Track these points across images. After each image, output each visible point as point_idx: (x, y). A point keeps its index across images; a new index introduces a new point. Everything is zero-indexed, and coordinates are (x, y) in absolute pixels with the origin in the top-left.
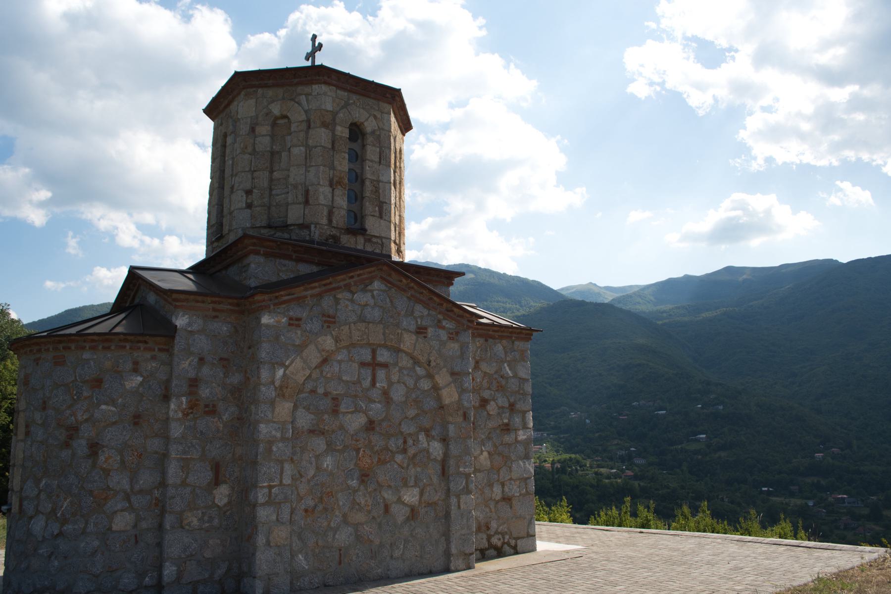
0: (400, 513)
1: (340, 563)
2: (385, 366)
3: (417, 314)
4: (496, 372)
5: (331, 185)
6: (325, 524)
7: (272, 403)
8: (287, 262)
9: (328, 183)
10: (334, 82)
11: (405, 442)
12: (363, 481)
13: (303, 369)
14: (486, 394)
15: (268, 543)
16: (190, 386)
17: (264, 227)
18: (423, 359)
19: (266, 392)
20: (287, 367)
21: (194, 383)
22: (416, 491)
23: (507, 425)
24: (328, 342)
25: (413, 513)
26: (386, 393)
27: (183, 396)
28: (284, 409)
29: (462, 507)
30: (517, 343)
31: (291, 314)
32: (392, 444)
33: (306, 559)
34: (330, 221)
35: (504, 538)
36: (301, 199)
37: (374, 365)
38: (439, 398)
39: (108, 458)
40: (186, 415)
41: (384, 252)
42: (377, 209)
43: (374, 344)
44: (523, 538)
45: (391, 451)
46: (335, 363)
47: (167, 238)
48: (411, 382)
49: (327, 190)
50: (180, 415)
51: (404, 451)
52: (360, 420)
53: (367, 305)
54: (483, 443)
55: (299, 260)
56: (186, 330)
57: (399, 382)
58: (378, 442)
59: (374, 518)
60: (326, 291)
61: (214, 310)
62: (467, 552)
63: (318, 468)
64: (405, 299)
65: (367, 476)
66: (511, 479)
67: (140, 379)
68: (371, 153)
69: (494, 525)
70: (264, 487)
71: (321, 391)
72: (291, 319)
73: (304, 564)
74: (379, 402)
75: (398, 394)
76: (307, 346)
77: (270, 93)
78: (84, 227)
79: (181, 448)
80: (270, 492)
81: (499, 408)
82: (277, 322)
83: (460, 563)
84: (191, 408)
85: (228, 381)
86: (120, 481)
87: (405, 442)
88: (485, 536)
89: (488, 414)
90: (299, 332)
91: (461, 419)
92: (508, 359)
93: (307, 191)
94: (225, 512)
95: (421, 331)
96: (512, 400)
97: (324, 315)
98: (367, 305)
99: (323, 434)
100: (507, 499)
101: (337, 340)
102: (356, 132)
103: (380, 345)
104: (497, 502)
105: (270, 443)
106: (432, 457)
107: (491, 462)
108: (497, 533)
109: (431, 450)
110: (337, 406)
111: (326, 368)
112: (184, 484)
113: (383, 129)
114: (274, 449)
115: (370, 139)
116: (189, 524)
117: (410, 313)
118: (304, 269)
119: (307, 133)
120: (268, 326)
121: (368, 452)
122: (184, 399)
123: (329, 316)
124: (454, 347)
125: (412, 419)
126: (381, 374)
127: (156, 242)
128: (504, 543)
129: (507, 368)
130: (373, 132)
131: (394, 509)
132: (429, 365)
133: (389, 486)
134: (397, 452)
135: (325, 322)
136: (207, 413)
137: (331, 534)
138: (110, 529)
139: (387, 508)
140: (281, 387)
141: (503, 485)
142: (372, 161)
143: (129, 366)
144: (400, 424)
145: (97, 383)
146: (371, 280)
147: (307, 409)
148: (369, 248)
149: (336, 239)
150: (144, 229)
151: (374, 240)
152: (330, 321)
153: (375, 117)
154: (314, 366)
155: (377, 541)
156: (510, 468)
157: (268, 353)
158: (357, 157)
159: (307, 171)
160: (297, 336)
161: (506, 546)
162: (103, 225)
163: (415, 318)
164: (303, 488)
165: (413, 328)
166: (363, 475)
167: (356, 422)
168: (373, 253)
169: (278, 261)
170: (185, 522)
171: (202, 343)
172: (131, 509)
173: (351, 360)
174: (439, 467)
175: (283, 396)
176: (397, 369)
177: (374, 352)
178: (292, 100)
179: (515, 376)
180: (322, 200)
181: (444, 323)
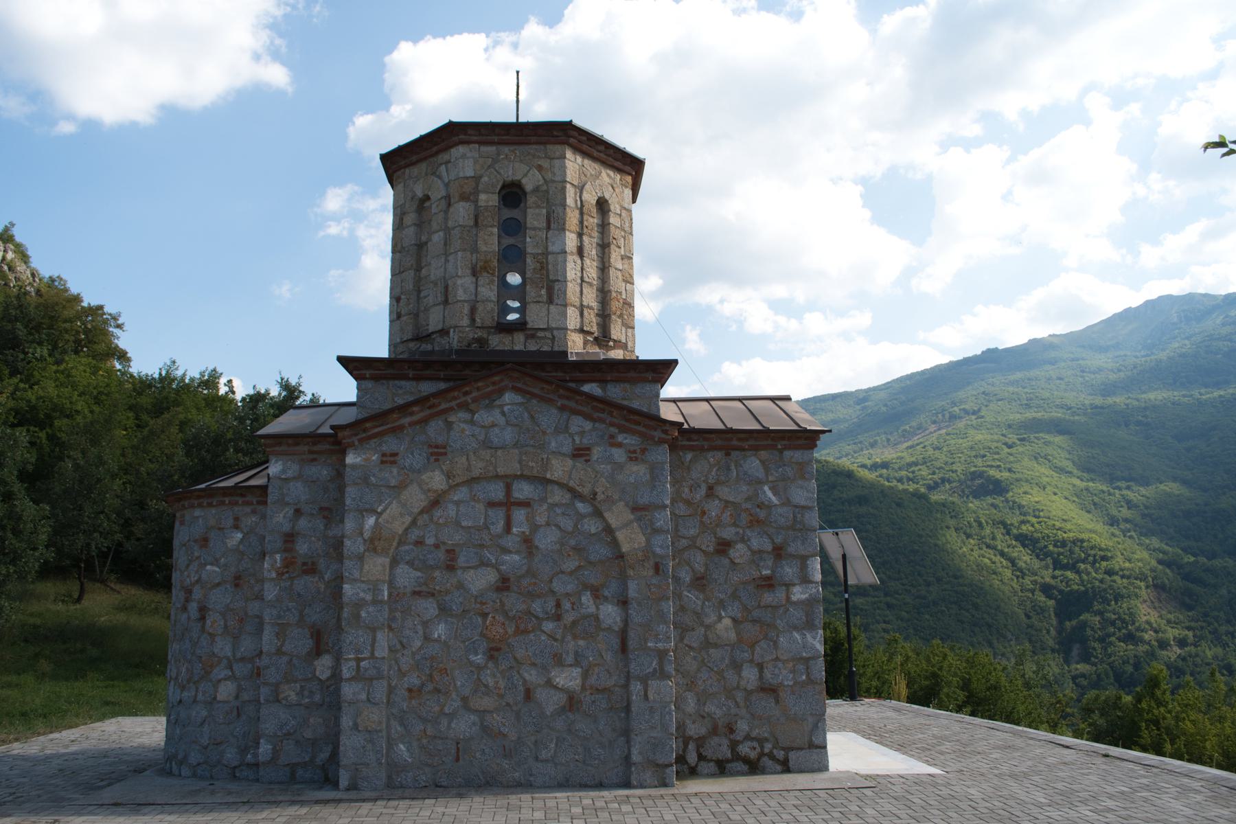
0: (550, 702)
1: (457, 760)
2: (525, 504)
3: (573, 429)
4: (748, 499)
5: (474, 273)
6: (437, 709)
7: (360, 558)
8: (403, 383)
9: (469, 272)
10: (475, 138)
11: (558, 605)
12: (491, 657)
13: (402, 515)
14: (728, 533)
15: (356, 726)
16: (286, 542)
17: (412, 340)
18: (586, 491)
19: (352, 546)
20: (380, 514)
21: (290, 538)
22: (576, 672)
23: (769, 578)
24: (437, 480)
25: (572, 702)
26: (527, 541)
27: (277, 552)
28: (376, 566)
29: (651, 697)
30: (788, 454)
31: (384, 448)
32: (537, 607)
33: (408, 750)
34: (473, 320)
35: (762, 747)
36: (440, 298)
37: (509, 504)
38: (615, 543)
39: (214, 621)
40: (280, 574)
41: (556, 349)
42: (543, 292)
43: (506, 476)
44: (802, 749)
45: (537, 618)
46: (450, 506)
47: (807, 316)
48: (567, 524)
49: (468, 281)
50: (274, 575)
51: (558, 618)
52: (487, 577)
53: (494, 425)
54: (722, 604)
55: (418, 378)
56: (280, 479)
57: (548, 524)
58: (514, 603)
59: (508, 704)
60: (432, 416)
61: (311, 452)
62: (661, 762)
63: (427, 638)
64: (555, 411)
65: (498, 650)
66: (777, 659)
67: (240, 535)
68: (534, 217)
69: (742, 727)
70: (350, 659)
71: (430, 541)
72: (384, 455)
73: (406, 755)
74: (518, 552)
75: (547, 540)
76: (406, 486)
77: (415, 171)
78: (701, 315)
79: (275, 612)
80: (358, 666)
81: (754, 552)
82: (366, 460)
83: (648, 776)
84: (287, 567)
85: (330, 533)
86: (223, 647)
87: (558, 605)
88: (725, 742)
89: (732, 562)
90: (395, 471)
91: (651, 572)
92: (770, 478)
93: (446, 287)
94: (328, 687)
95: (581, 453)
96: (779, 540)
97: (430, 446)
98: (494, 425)
99: (433, 595)
100: (771, 690)
101: (449, 476)
102: (512, 194)
103: (516, 477)
104: (749, 693)
105: (359, 604)
106: (604, 626)
107: (738, 634)
108: (748, 737)
109: (601, 617)
110: (452, 560)
111: (438, 513)
112: (279, 652)
113: (554, 181)
114: (363, 614)
115: (531, 200)
116: (286, 698)
117: (563, 429)
118: (427, 388)
119: (446, 212)
120: (354, 467)
121: (500, 618)
122: (278, 557)
123: (437, 447)
124: (638, 471)
125: (571, 573)
126: (519, 515)
127: (794, 324)
128: (762, 754)
129: (770, 494)
130: (536, 190)
131: (541, 695)
132: (594, 499)
133: (534, 665)
134: (547, 619)
135: (432, 454)
136: (306, 572)
137: (445, 722)
138: (215, 698)
139: (528, 695)
140: (372, 540)
141: (761, 667)
142: (534, 229)
143: (230, 522)
144: (551, 581)
145: (204, 541)
146: (501, 392)
147: (410, 563)
148: (532, 347)
149: (482, 342)
150: (776, 306)
151: (540, 334)
152: (438, 453)
153: (540, 168)
154: (416, 511)
155: (513, 736)
156: (775, 643)
157: (354, 499)
158: (512, 228)
159: (447, 261)
160: (392, 475)
161: (765, 759)
162: (728, 309)
163: (571, 435)
164: (406, 661)
165: (567, 448)
166: (492, 649)
167: (480, 581)
168: (539, 352)
169: (391, 382)
170: (282, 696)
171: (298, 491)
172: (233, 677)
173: (474, 498)
174: (615, 642)
175: (375, 550)
176: (545, 507)
177: (508, 488)
178: (434, 174)
179: (787, 502)
180: (461, 295)
181: (620, 438)
